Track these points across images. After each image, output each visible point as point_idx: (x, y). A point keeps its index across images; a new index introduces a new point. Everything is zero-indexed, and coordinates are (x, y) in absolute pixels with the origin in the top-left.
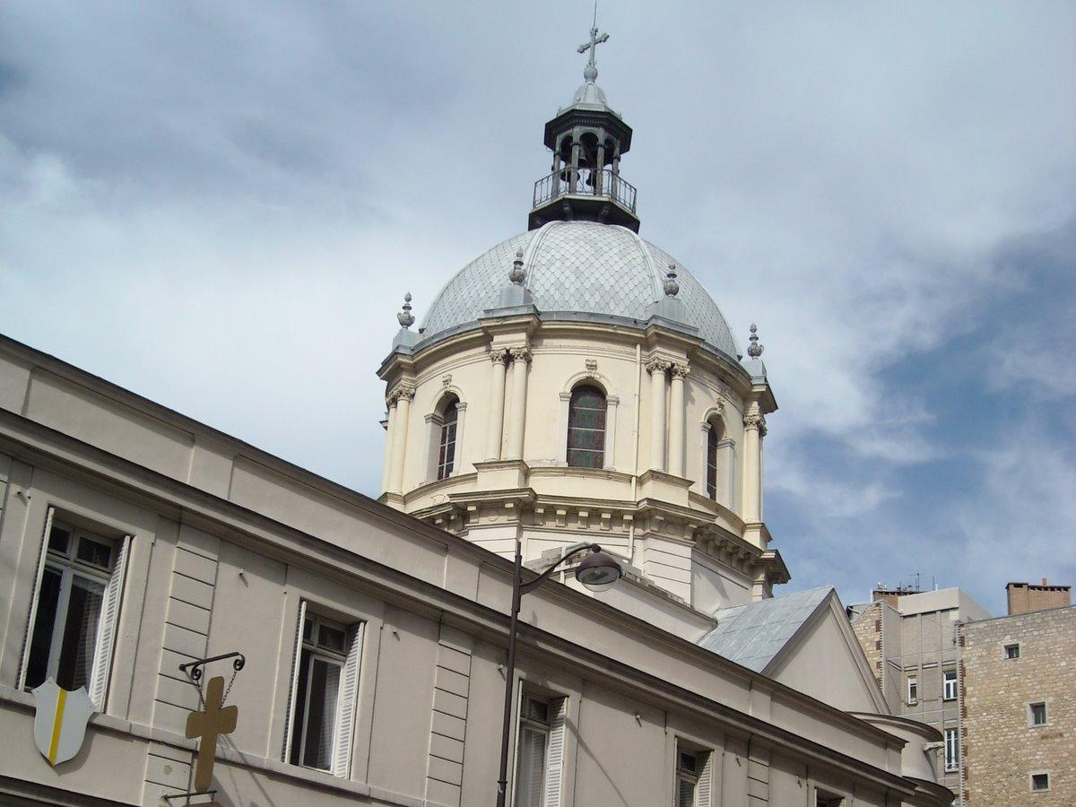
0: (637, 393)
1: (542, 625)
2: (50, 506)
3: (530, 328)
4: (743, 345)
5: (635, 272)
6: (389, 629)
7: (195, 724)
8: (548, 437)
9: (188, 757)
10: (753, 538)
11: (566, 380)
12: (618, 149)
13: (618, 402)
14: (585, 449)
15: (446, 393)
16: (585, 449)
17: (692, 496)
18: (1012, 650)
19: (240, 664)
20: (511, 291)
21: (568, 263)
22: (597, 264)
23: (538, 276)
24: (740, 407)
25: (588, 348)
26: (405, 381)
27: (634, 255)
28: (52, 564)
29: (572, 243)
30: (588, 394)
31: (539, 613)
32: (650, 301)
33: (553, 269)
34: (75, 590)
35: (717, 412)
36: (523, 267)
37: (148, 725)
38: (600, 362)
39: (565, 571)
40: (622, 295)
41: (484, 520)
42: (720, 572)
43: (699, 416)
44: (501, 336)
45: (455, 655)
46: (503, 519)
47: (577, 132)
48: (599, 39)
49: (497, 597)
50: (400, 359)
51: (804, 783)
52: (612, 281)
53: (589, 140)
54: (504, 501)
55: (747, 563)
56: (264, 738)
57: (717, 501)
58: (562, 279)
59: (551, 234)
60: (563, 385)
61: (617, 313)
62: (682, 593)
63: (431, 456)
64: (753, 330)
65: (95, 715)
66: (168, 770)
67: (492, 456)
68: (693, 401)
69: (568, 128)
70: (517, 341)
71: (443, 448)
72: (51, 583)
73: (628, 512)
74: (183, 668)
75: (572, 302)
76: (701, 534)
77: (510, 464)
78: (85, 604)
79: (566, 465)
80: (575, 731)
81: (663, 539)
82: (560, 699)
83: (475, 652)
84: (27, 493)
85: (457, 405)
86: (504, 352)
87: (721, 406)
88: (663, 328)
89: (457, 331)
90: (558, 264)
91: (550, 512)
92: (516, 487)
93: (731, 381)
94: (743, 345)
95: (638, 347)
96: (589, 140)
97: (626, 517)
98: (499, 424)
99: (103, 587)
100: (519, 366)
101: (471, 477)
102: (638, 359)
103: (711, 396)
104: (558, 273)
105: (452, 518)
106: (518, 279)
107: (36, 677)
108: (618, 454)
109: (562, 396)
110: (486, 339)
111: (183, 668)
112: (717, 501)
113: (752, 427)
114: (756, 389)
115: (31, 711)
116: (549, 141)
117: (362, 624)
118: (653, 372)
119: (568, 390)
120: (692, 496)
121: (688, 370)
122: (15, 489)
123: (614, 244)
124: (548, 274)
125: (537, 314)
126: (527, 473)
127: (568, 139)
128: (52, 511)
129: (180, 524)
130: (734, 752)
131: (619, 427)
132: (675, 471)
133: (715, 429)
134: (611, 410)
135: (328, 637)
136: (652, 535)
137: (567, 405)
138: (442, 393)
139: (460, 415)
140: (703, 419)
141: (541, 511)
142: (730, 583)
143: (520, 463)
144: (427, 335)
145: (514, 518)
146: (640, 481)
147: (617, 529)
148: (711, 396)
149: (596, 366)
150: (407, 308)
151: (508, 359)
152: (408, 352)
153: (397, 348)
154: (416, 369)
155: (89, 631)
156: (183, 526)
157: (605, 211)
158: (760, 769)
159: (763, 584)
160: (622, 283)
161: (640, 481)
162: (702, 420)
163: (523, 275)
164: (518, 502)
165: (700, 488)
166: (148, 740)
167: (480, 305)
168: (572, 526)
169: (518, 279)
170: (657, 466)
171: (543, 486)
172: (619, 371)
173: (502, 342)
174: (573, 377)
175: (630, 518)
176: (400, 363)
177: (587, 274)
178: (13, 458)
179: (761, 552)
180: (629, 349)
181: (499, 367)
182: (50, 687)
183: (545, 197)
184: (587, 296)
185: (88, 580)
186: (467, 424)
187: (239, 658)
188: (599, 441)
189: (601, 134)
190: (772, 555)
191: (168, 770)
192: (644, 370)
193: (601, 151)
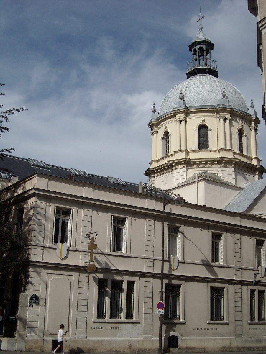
0: (216, 126)
1: (173, 212)
2: (55, 206)
3: (185, 112)
4: (249, 105)
5: (214, 91)
6: (133, 218)
7: (89, 247)
8: (193, 142)
9: (89, 253)
10: (254, 162)
11: (197, 125)
12: (210, 50)
13: (211, 130)
14: (203, 145)
15: (165, 131)
16: (203, 145)
17: (234, 153)
19: (97, 235)
20: (179, 102)
21: (195, 91)
22: (203, 90)
23: (187, 96)
24: (249, 124)
25: (202, 115)
26: (155, 128)
27: (214, 85)
28: (57, 217)
29: (196, 84)
30: (203, 129)
32: (219, 99)
33: (191, 93)
34: (62, 222)
35: (241, 128)
36: (182, 94)
37: (80, 248)
38: (205, 119)
39: (197, 181)
40: (210, 98)
41: (177, 167)
42: (245, 173)
43: (235, 130)
45: (150, 222)
46: (182, 166)
47: (197, 47)
50: (153, 122)
51: (252, 238)
52: (207, 95)
53: (201, 49)
55: (253, 169)
56: (106, 247)
57: (243, 154)
58: (194, 96)
59: (191, 82)
61: (209, 104)
62: (233, 181)
63: (163, 149)
65: (69, 248)
66: (85, 257)
67: (178, 149)
68: (233, 126)
69: (194, 47)
70: (182, 116)
71: (166, 146)
72: (57, 221)
73: (216, 161)
74: (86, 235)
75: (197, 102)
76: (237, 164)
77: (183, 151)
78: (65, 224)
79: (198, 149)
80: (183, 234)
81: (226, 167)
82: (179, 227)
83: (155, 220)
84: (50, 204)
85: (168, 135)
86: (179, 119)
87: (242, 126)
88: (222, 108)
89: (166, 114)
90: (192, 91)
91: (194, 163)
92: (185, 157)
94: (249, 105)
95: (216, 113)
96: (201, 49)
97: (215, 162)
98: (179, 140)
99: (68, 220)
100: (183, 123)
101: (173, 155)
102: (216, 117)
103: (239, 124)
104: (192, 95)
105: (169, 167)
107: (56, 241)
110: (174, 116)
111: (86, 235)
112: (243, 154)
113: (252, 129)
114: (253, 119)
115: (56, 249)
116: (191, 50)
117: (127, 219)
118: (220, 120)
119: (197, 128)
121: (230, 118)
122: (48, 204)
123: (208, 83)
124: (190, 95)
125: (187, 107)
126: (188, 153)
127: (195, 50)
128: (56, 207)
129: (83, 204)
130: (230, 233)
132: (228, 147)
133: (240, 133)
134: (209, 132)
135: (118, 225)
136: (222, 167)
137: (197, 132)
138: (164, 132)
139: (169, 137)
140: (236, 130)
141: (192, 163)
142: (248, 176)
143: (186, 150)
144: (160, 114)
145: (185, 166)
146: (219, 151)
147: (213, 166)
148: (239, 124)
149: (204, 120)
151: (180, 121)
152: (155, 120)
153: (152, 119)
154: (157, 125)
155: (67, 229)
156: (83, 205)
157: (207, 70)
158: (237, 236)
159: (258, 174)
160: (210, 95)
161: (219, 151)
162: (236, 131)
163: (182, 97)
164: (185, 161)
165: (237, 150)
166: (80, 251)
167: (172, 106)
168: (201, 166)
169: (182, 98)
170: (223, 147)
171: (192, 156)
172: (211, 121)
173: (178, 116)
175: (216, 162)
176: (153, 124)
177: (200, 94)
178: (46, 198)
179: (257, 166)
180: (213, 114)
181: (178, 124)
182: (59, 243)
184: (201, 100)
185: (65, 219)
186: (171, 139)
187: (96, 233)
188: (207, 141)
189: (204, 47)
190: (259, 167)
191: (85, 257)
192: (218, 119)
193: (205, 52)
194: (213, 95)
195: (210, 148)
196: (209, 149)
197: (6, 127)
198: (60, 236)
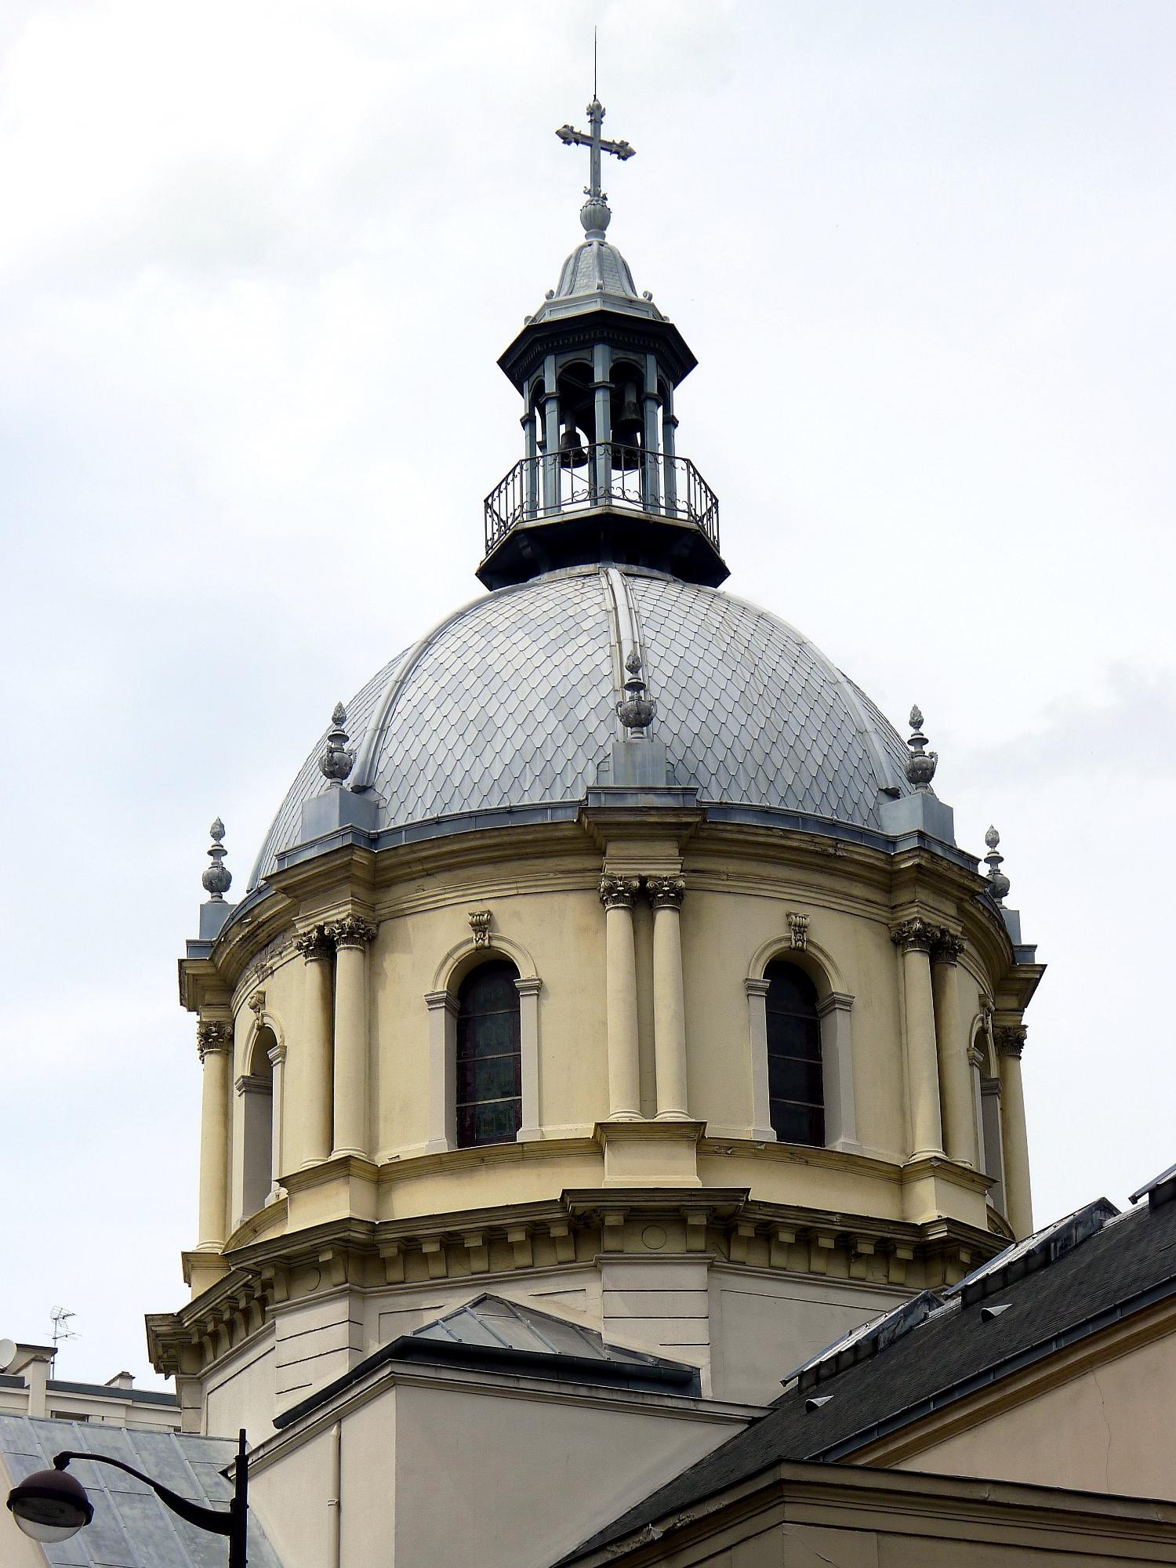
14: (484, 1109)
16: (484, 1109)
30: (484, 994)
41: (635, 1245)
44: (755, 864)
54: (316, 1251)
60: (431, 977)
64: (218, 833)
70: (660, 864)
79: (771, 1135)
93: (267, 929)
108: (858, 1120)
119: (758, 974)
131: (855, 1050)
132: (966, 1155)
134: (527, 1005)
150: (217, 852)
173: (629, 862)
174: (449, 955)
194: (450, 742)
195: (840, 1142)
196: (522, 1136)
197: (1000, 888)
198: (697, 1517)
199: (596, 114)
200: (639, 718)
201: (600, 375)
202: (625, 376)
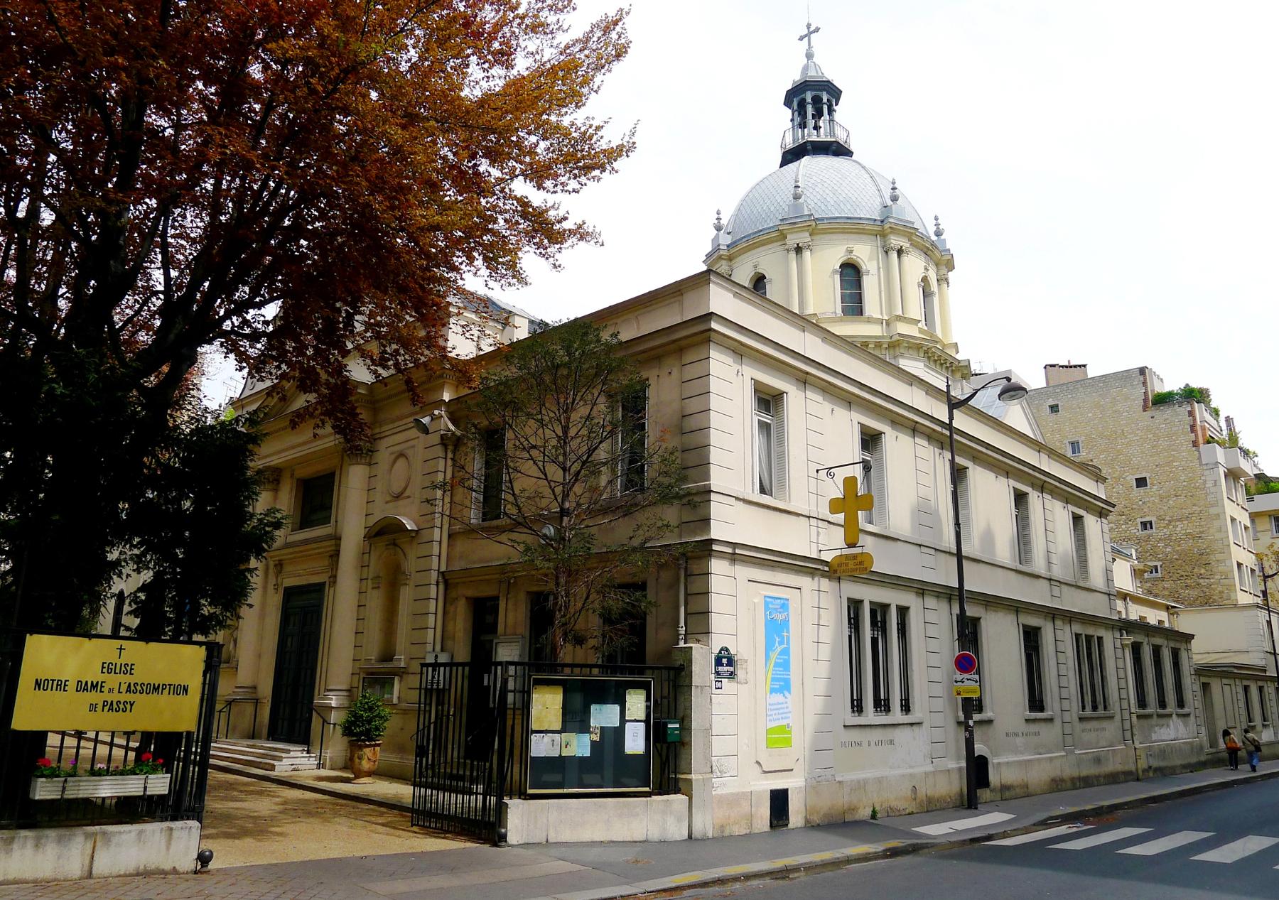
18: (1054, 409)
31: (962, 421)
48: (811, 31)
49: (941, 412)
64: (936, 219)
106: (797, 197)
109: (834, 272)
116: (788, 103)
120: (921, 331)
127: (804, 100)
150: (719, 219)
183: (790, 144)
199: (817, 30)
200: (797, 197)
201: (809, 100)
202: (817, 101)
